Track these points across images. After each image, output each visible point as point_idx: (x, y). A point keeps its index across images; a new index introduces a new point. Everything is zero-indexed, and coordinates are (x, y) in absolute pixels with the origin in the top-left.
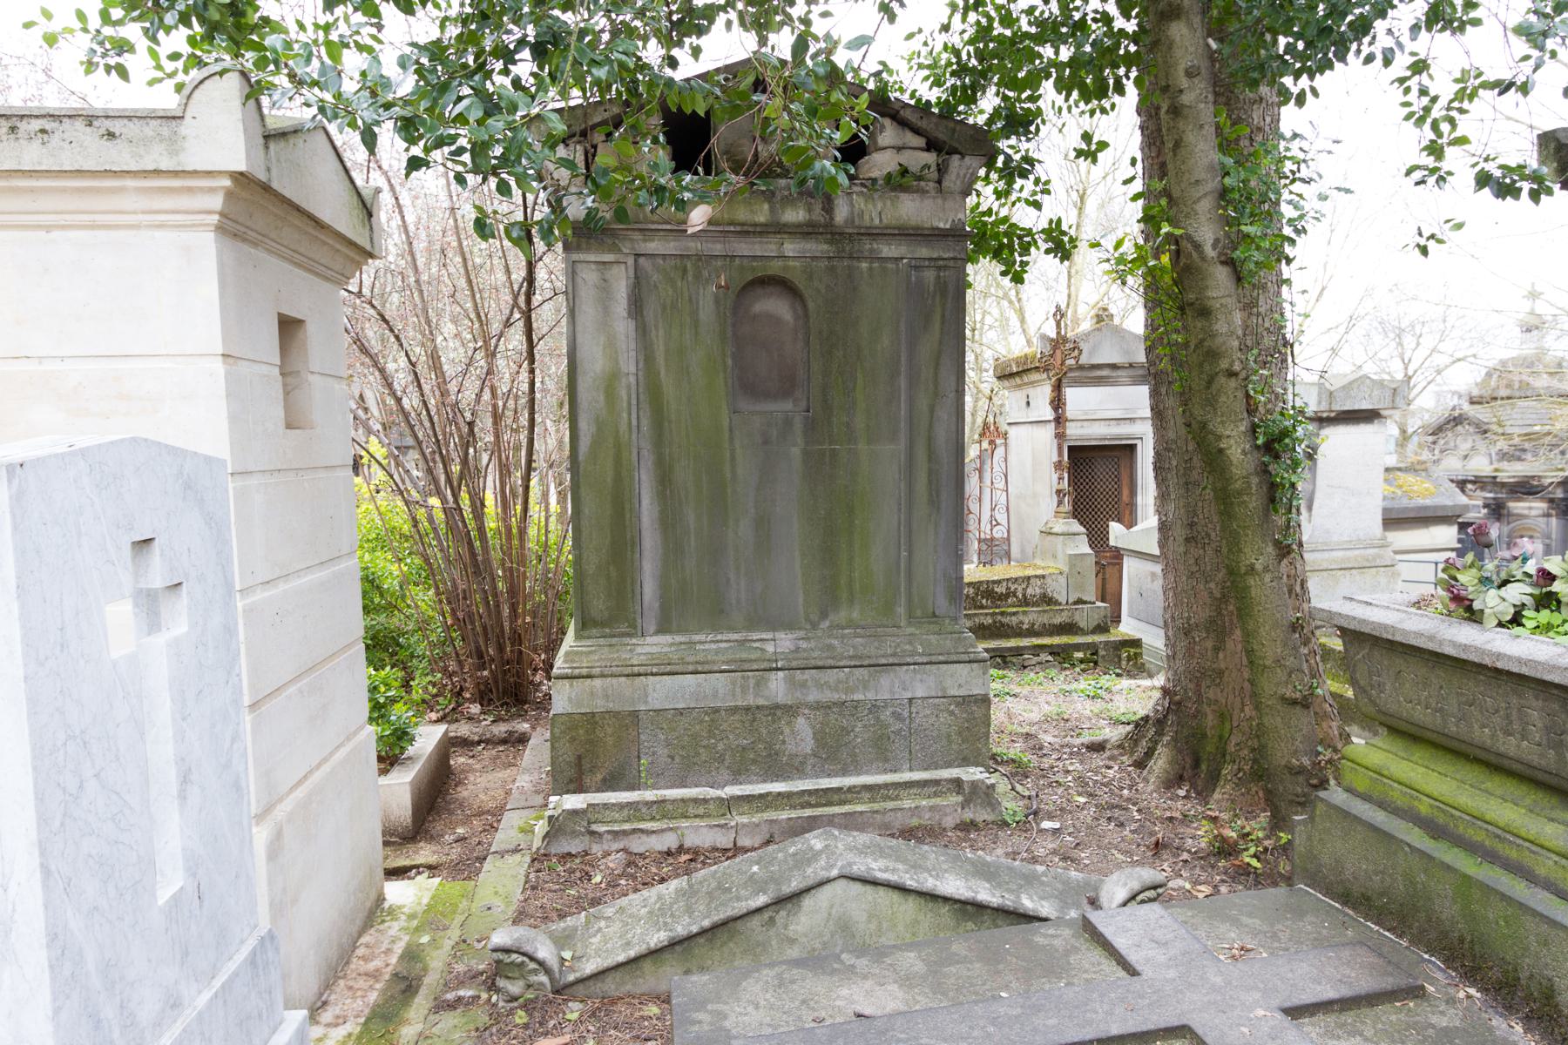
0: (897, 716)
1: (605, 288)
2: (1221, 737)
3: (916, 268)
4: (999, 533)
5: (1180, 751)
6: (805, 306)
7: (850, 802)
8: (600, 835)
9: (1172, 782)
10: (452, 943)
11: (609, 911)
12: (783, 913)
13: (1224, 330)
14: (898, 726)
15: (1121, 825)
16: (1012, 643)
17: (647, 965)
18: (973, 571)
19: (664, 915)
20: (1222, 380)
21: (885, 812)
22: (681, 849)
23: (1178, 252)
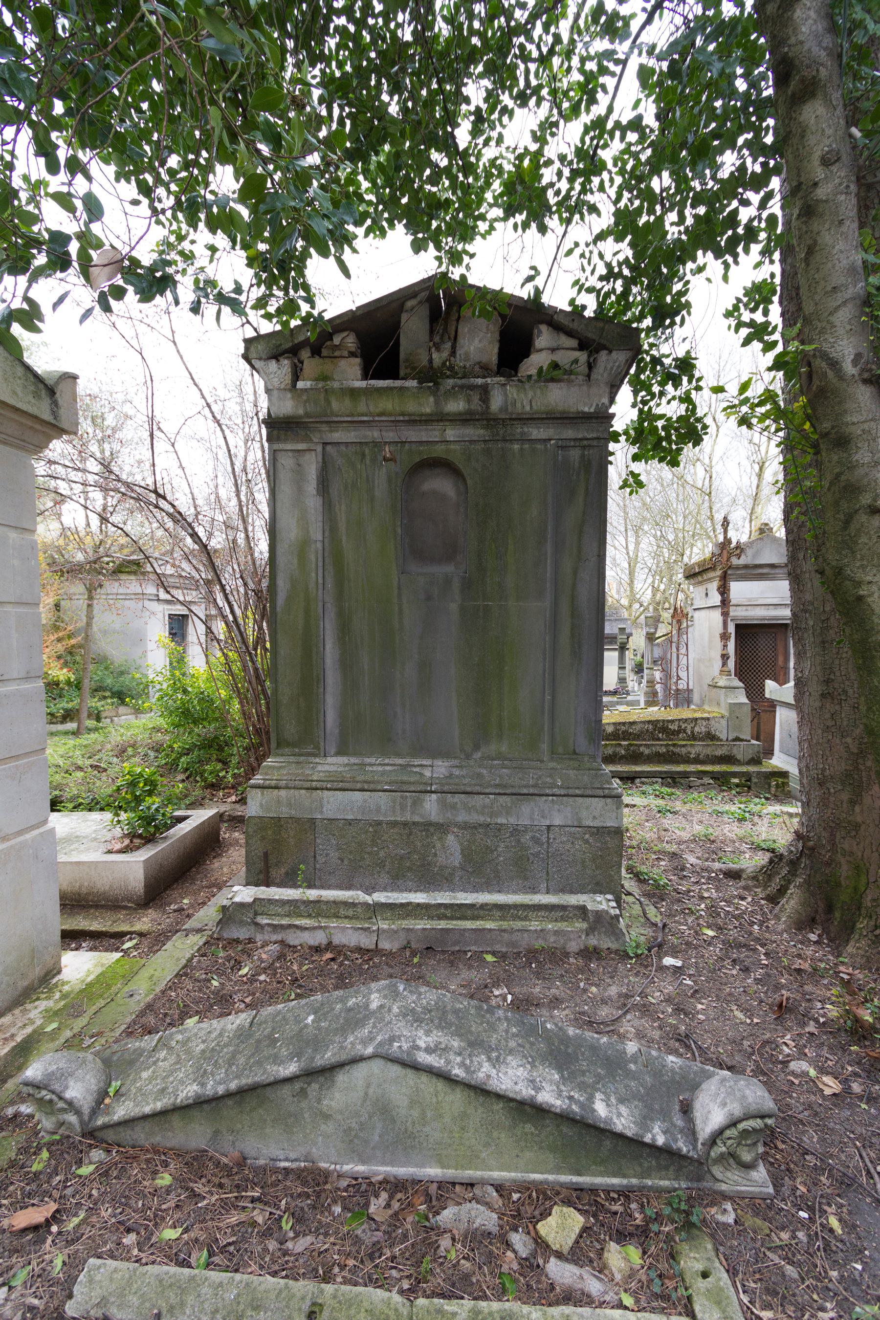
0: (536, 841)
1: (299, 472)
2: (856, 889)
3: (562, 447)
4: (682, 685)
5: (813, 894)
6: (464, 480)
7: (482, 918)
9: (804, 923)
12: (315, 1086)
13: (866, 460)
14: (537, 849)
15: (746, 970)
16: (681, 768)
18: (609, 717)
20: (863, 518)
21: (512, 931)
23: (810, 375)
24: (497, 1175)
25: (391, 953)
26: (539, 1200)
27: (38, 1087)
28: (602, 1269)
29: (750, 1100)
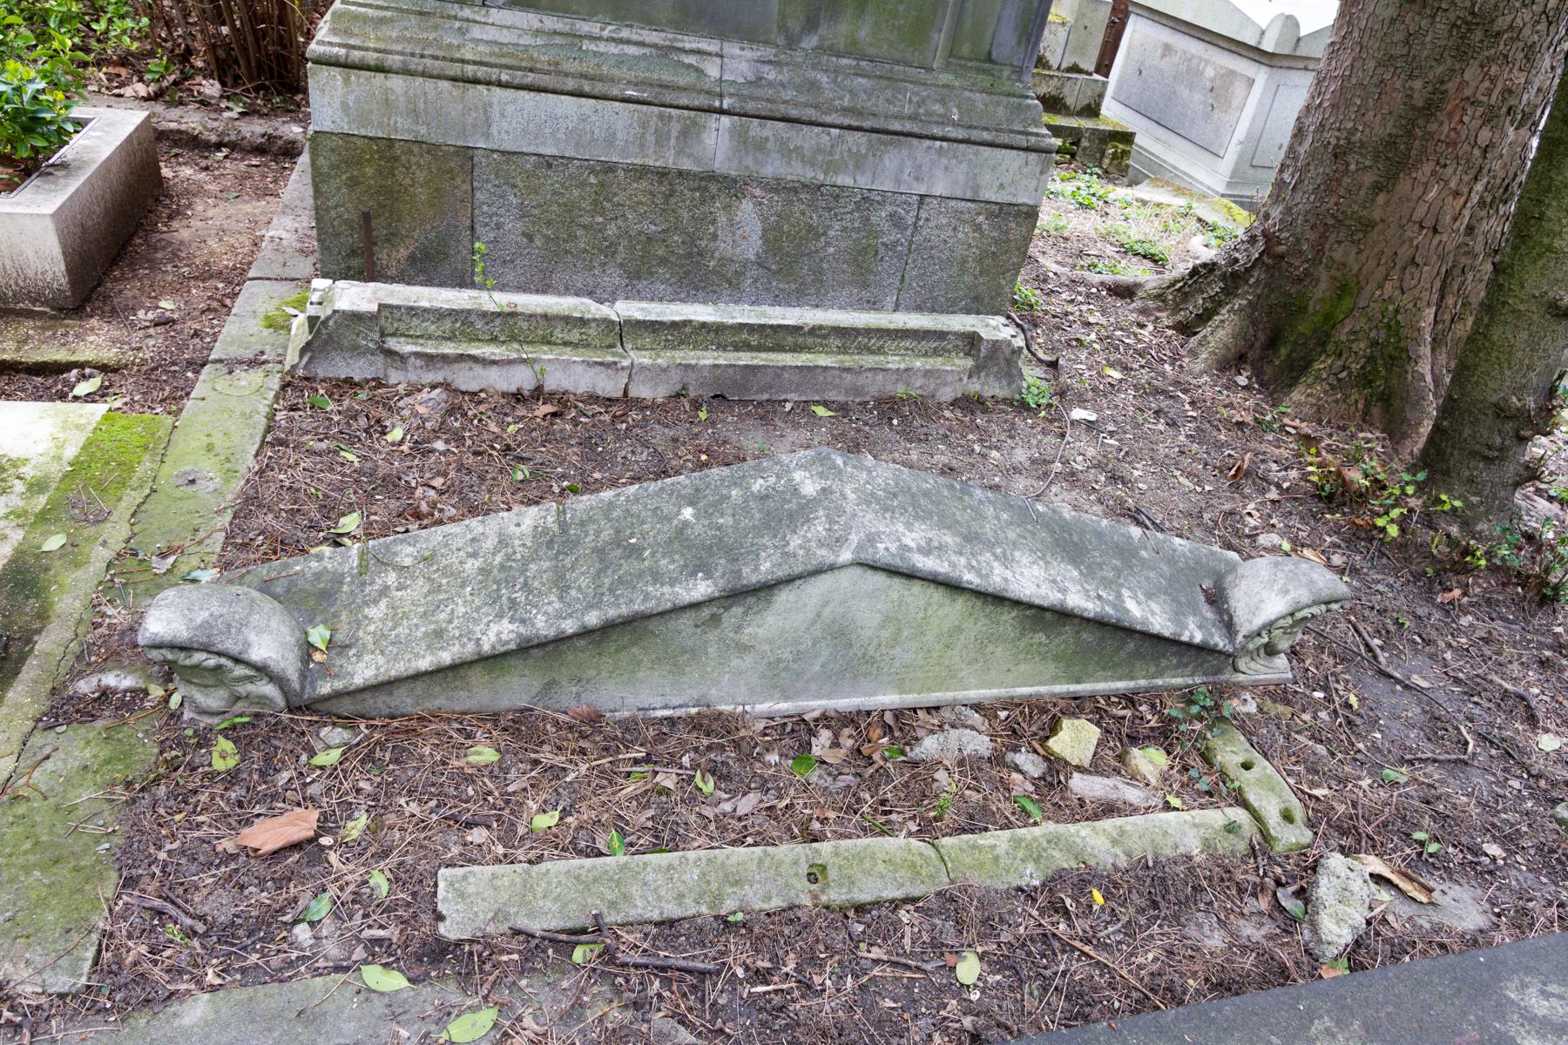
0: (896, 221)
8: (403, 358)
10: (108, 554)
11: (406, 554)
12: (737, 610)
17: (476, 676)
19: (510, 582)
21: (861, 370)
22: (538, 393)
24: (974, 694)
25: (654, 406)
26: (1041, 719)
27: (182, 648)
28: (1134, 778)
29: (1321, 585)
